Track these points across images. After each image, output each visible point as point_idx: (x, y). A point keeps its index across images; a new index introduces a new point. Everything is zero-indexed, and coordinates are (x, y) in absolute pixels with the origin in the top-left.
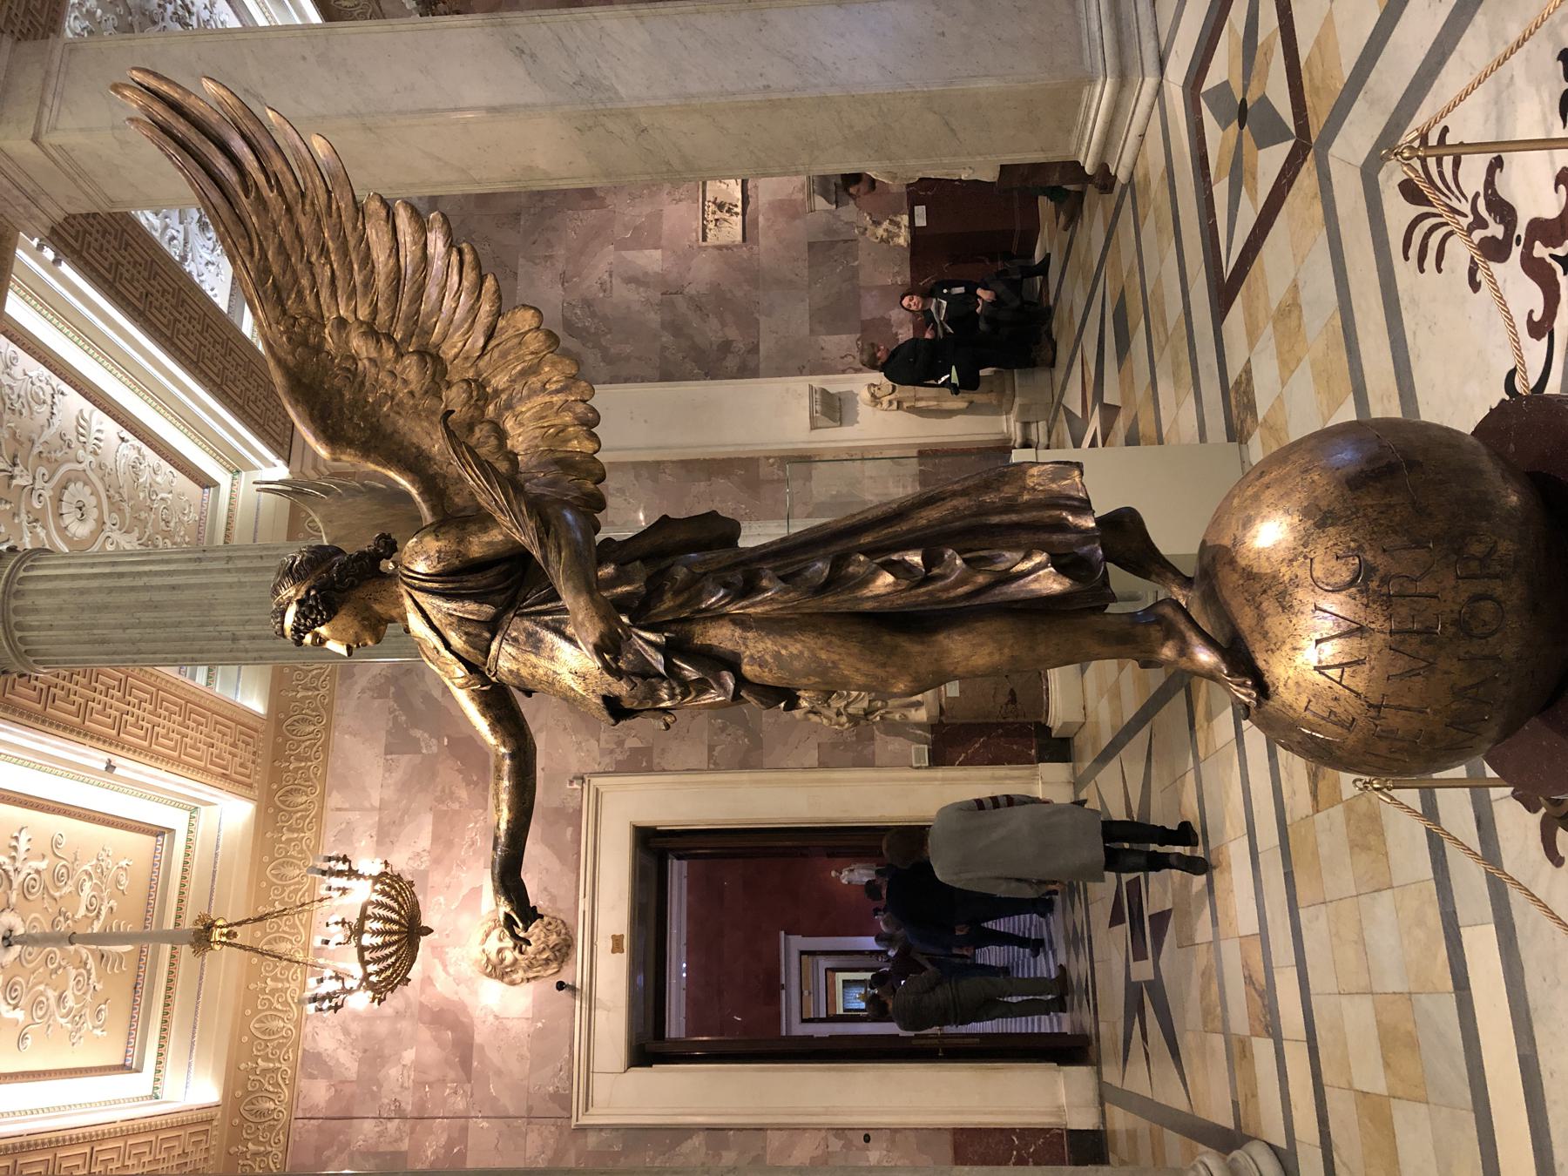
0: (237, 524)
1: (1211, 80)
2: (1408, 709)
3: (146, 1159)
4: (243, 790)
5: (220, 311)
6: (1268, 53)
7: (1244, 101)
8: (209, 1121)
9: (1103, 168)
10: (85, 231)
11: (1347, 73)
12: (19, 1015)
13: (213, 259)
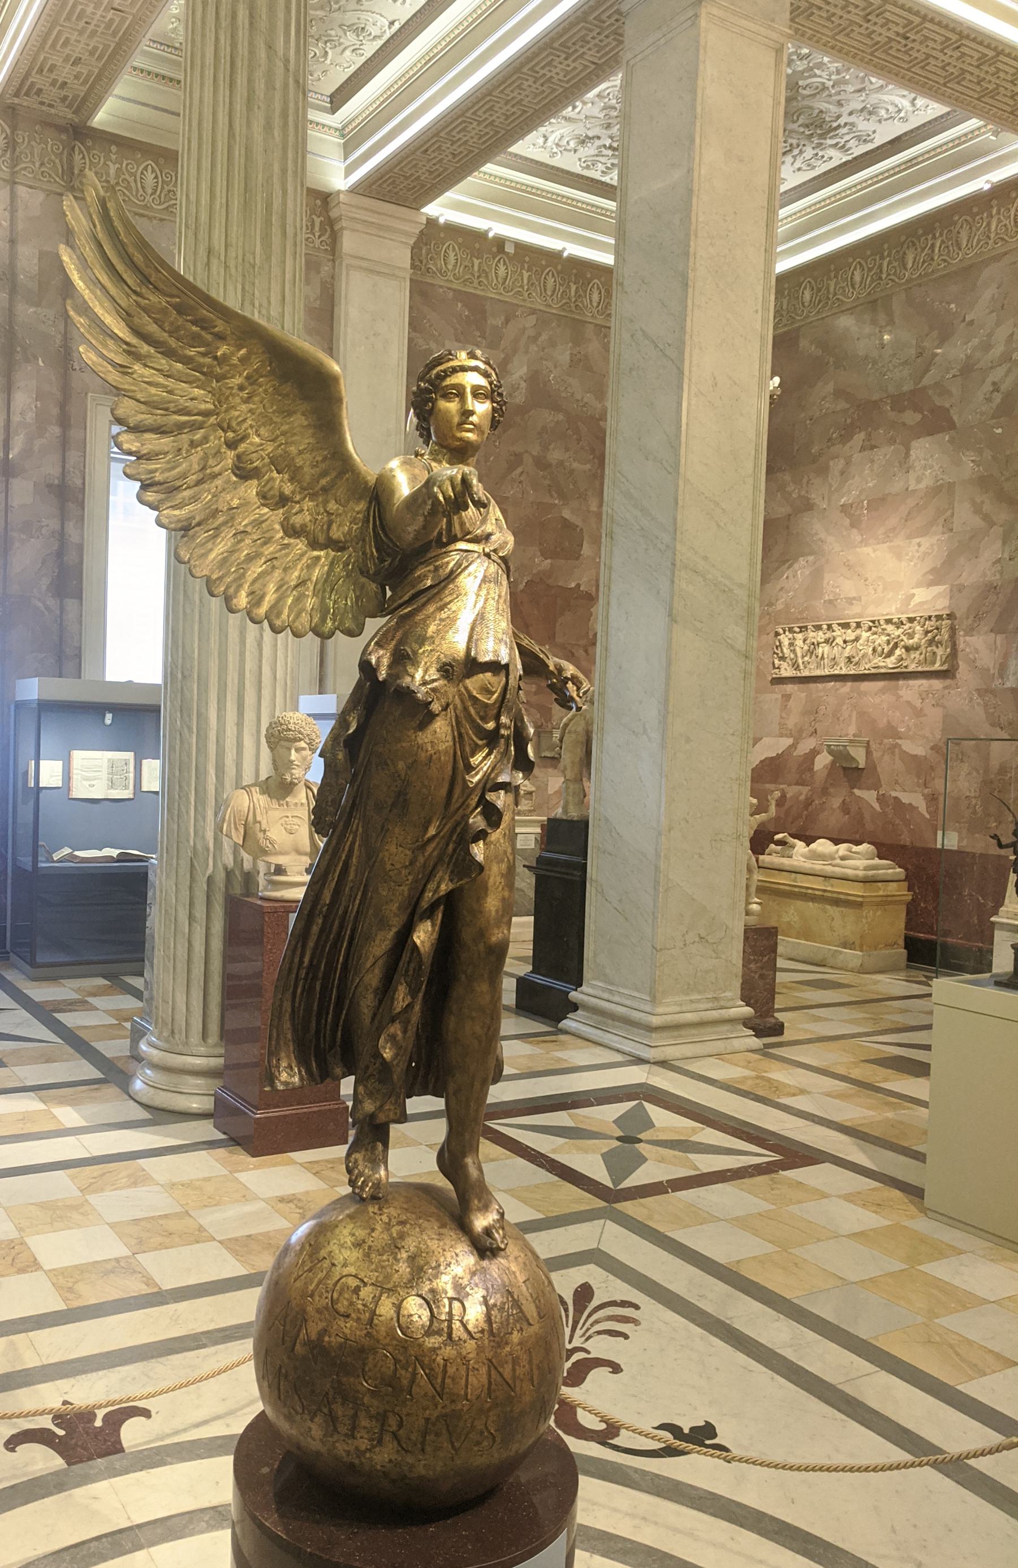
1: (656, 1113)
4: (16, 84)
5: (510, 146)
7: (640, 1141)
9: (575, 1007)
10: (603, 29)
13: (549, 143)
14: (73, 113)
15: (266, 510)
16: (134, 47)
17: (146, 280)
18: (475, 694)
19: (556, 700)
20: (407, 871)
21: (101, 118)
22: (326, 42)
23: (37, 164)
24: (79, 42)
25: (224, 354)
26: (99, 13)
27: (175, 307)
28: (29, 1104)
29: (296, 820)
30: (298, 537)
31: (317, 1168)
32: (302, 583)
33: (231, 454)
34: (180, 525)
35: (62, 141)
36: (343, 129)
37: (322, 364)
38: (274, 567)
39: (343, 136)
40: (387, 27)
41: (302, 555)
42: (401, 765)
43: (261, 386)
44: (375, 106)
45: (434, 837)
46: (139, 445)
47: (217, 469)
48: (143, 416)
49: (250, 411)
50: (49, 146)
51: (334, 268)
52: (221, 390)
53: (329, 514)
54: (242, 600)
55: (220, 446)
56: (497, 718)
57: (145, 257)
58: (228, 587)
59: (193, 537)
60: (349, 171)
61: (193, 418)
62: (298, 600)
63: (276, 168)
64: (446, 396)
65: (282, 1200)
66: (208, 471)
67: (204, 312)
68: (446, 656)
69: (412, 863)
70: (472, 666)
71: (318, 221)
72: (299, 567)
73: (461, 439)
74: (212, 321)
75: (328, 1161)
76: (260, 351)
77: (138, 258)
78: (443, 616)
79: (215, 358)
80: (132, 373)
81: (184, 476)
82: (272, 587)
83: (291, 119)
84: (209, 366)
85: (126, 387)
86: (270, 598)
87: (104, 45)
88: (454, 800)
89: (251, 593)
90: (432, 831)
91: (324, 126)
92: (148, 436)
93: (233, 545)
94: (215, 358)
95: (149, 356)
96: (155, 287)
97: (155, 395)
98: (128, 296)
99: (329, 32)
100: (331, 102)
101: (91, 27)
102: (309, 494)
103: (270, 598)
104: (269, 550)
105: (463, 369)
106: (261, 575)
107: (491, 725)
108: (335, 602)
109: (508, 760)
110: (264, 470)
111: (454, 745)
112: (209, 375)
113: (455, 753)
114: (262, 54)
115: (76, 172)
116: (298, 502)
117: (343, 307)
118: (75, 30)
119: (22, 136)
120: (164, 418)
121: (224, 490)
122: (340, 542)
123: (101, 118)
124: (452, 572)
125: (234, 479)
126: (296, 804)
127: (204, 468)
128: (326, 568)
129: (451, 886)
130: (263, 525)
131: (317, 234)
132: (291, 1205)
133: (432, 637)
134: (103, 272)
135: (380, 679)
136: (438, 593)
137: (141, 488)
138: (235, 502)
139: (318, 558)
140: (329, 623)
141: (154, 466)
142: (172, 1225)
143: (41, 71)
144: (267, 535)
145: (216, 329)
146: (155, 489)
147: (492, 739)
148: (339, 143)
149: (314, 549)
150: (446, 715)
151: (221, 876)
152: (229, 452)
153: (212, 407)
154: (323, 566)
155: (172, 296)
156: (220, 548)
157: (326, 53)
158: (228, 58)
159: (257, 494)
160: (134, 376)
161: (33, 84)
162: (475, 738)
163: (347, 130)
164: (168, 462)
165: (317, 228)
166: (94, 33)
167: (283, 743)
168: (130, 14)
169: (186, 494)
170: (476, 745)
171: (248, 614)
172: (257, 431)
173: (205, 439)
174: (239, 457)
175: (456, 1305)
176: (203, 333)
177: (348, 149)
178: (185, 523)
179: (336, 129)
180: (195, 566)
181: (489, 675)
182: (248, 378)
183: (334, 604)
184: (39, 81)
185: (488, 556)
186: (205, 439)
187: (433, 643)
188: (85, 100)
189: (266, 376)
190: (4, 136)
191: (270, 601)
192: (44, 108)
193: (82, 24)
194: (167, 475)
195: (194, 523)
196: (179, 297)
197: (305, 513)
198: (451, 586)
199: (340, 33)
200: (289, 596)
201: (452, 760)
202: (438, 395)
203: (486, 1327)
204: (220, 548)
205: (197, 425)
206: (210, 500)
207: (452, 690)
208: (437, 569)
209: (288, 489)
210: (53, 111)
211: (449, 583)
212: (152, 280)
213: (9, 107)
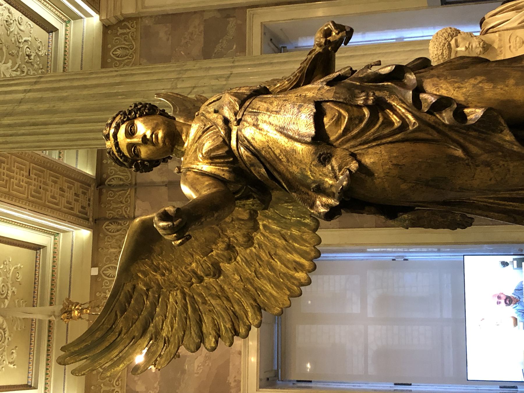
0: (59, 262)
4: (82, 221)
14: (88, 191)
15: (238, 258)
16: (48, 160)
17: (111, 329)
18: (340, 131)
19: (346, 44)
20: (495, 167)
21: (89, 171)
22: (19, 42)
23: (122, 205)
24: (51, 190)
25: (144, 286)
26: (33, 181)
27: (122, 313)
29: (512, 40)
30: (252, 238)
32: (284, 237)
33: (206, 279)
34: (258, 313)
35: (107, 192)
36: (65, 22)
37: (136, 232)
38: (275, 254)
39: (69, 21)
40: (2, 7)
41: (264, 236)
42: (404, 186)
43: (159, 264)
44: (47, 5)
45: (465, 149)
46: (211, 336)
47: (218, 288)
48: (193, 333)
49: (176, 268)
50: (111, 199)
51: (146, 17)
52: (167, 287)
53: (232, 220)
54: (301, 275)
55: (203, 286)
56: (360, 107)
57: (97, 330)
58: (293, 284)
59: (263, 302)
60: (88, 15)
61: (188, 302)
62: (295, 240)
63: (85, 92)
64: (137, 155)
66: (220, 294)
67: (121, 297)
68: (314, 160)
69: (487, 164)
70: (320, 138)
71: (121, 31)
72: (272, 238)
73: (164, 142)
74: (125, 293)
76: (137, 265)
77: (98, 335)
78: (284, 160)
79: (148, 290)
80: (168, 338)
81: (226, 309)
82: (289, 256)
83: (56, 85)
84: (153, 293)
85: (177, 342)
86: (297, 258)
87: (50, 176)
88: (430, 137)
89: (295, 269)
90: (459, 153)
91: (66, 34)
92: (204, 330)
93: (265, 279)
94: (148, 290)
95: (156, 327)
96: (114, 324)
97: (178, 325)
98: (122, 339)
99: (13, 42)
100: (52, 32)
101: (42, 186)
102: (222, 233)
103: (297, 258)
104: (264, 256)
105: (117, 144)
106: (282, 263)
107: (366, 112)
108: (292, 216)
109: (395, 88)
110: (213, 260)
111: (384, 144)
112: (160, 292)
113: (391, 142)
114: (24, 107)
115: (121, 183)
116: (229, 239)
117: (167, 8)
118: (46, 194)
119: (109, 214)
120: (192, 319)
121: (230, 284)
122: (250, 212)
123: (89, 171)
124: (253, 154)
125: (222, 277)
126: (500, 40)
127: (219, 297)
128: (270, 221)
129: (507, 131)
130: (249, 260)
131: (128, 30)
133: (301, 169)
134: (113, 352)
135: (338, 203)
136: (269, 163)
137: (238, 335)
138: (237, 277)
139: (264, 226)
140: (307, 221)
141: (223, 327)
143: (72, 209)
144: (255, 258)
145: (130, 290)
146: (237, 327)
147: (379, 106)
148: (74, 23)
149: (259, 228)
150: (360, 154)
152: (206, 281)
153: (178, 291)
154: (269, 223)
155: (116, 315)
156: (269, 288)
157: (25, 41)
158: (32, 127)
159: (229, 263)
160: (169, 336)
161: (80, 212)
162: (377, 126)
163: (65, 19)
164: (219, 318)
165: (125, 31)
166: (45, 183)
168: (30, 166)
169: (237, 308)
170: (383, 123)
171: (310, 272)
172: (188, 265)
173: (200, 295)
174: (207, 275)
176: (134, 297)
177: (76, 17)
178: (256, 309)
179: (66, 26)
180: (283, 304)
181: (326, 120)
182: (156, 272)
183: (294, 217)
185: (239, 122)
186: (200, 295)
187: (305, 169)
188: (81, 182)
189: (152, 261)
190: (110, 224)
191: (299, 258)
192: (91, 203)
193: (41, 190)
194: (226, 320)
195: (254, 304)
196: (116, 312)
197: (237, 235)
198: (263, 153)
199: (12, 35)
200: (294, 246)
201: (397, 145)
202: (138, 159)
204: (269, 288)
205: (193, 299)
206: (238, 293)
207: (339, 153)
208: (252, 165)
209: (221, 245)
210: (92, 199)
211: (261, 154)
212: (109, 327)
213: (95, 222)
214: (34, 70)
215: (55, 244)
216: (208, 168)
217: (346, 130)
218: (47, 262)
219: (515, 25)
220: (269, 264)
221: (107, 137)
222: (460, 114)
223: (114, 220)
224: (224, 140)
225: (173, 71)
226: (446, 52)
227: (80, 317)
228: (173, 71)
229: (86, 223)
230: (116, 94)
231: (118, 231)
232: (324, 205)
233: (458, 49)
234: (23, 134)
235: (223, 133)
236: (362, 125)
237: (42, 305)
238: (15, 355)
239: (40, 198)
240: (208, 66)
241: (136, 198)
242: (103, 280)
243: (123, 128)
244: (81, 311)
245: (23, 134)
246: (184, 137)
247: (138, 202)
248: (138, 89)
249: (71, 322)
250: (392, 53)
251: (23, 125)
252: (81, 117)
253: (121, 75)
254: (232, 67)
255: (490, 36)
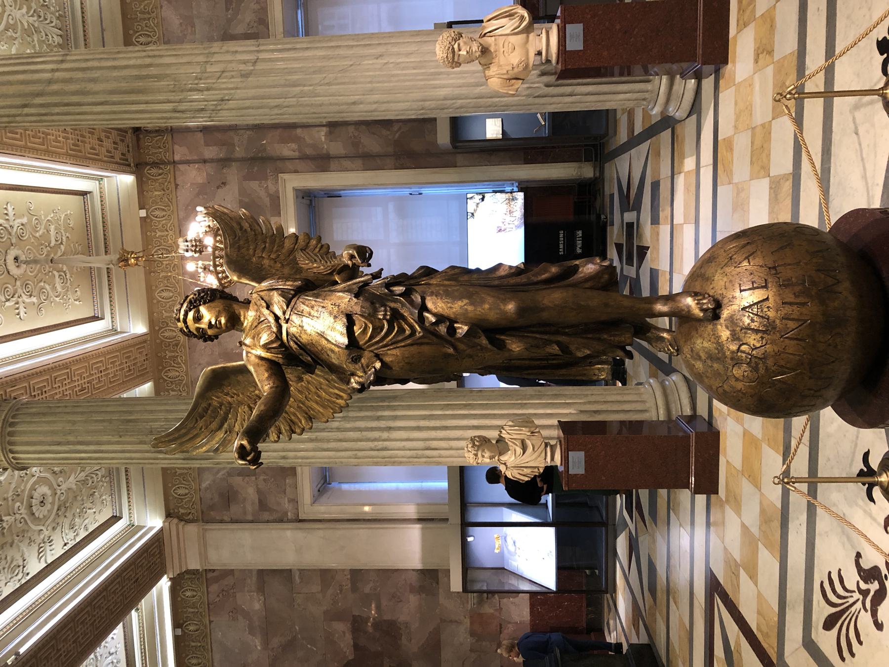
0: (108, 209)
2: (789, 265)
3: (117, 364)
4: (124, 168)
6: (738, 644)
8: (145, 342)
11: (776, 609)
12: (34, 299)
26: (70, 136)
28: (680, 181)
29: (506, 44)
31: (741, 22)
63: (115, 74)
65: (756, 61)
69: (470, 356)
70: (353, 342)
75: (739, 12)
82: (331, 390)
83: (84, 65)
90: (451, 351)
95: (229, 425)
103: (336, 391)
114: (55, 87)
119: (149, 159)
126: (496, 45)
132: (761, 56)
142: (758, 143)
143: (112, 157)
151: (545, 79)
167: (456, 59)
175: (744, 348)
184: (118, 157)
185: (287, 321)
192: (131, 149)
193: (80, 143)
203: (760, 335)
207: (367, 354)
214: (52, 13)
215: (100, 188)
216: (264, 354)
217: (371, 337)
218: (96, 203)
219: (508, 32)
220: (316, 393)
221: (179, 320)
222: (452, 330)
223: (155, 165)
224: (277, 336)
225: (201, 54)
226: (450, 56)
227: (137, 264)
228: (201, 54)
229: (128, 168)
230: (147, 77)
231: (160, 175)
232: (357, 383)
233: (461, 53)
234: (58, 114)
235: (275, 329)
236: (383, 333)
237: (97, 255)
238: (78, 293)
239: (80, 151)
240: (235, 49)
241: (174, 143)
242: (152, 220)
243: (191, 315)
244: (137, 259)
245: (58, 114)
246: (242, 319)
247: (176, 147)
248: (168, 72)
249: (128, 269)
250: (404, 43)
251: (56, 105)
252: (116, 98)
253: (149, 56)
254: (258, 51)
255: (489, 40)
